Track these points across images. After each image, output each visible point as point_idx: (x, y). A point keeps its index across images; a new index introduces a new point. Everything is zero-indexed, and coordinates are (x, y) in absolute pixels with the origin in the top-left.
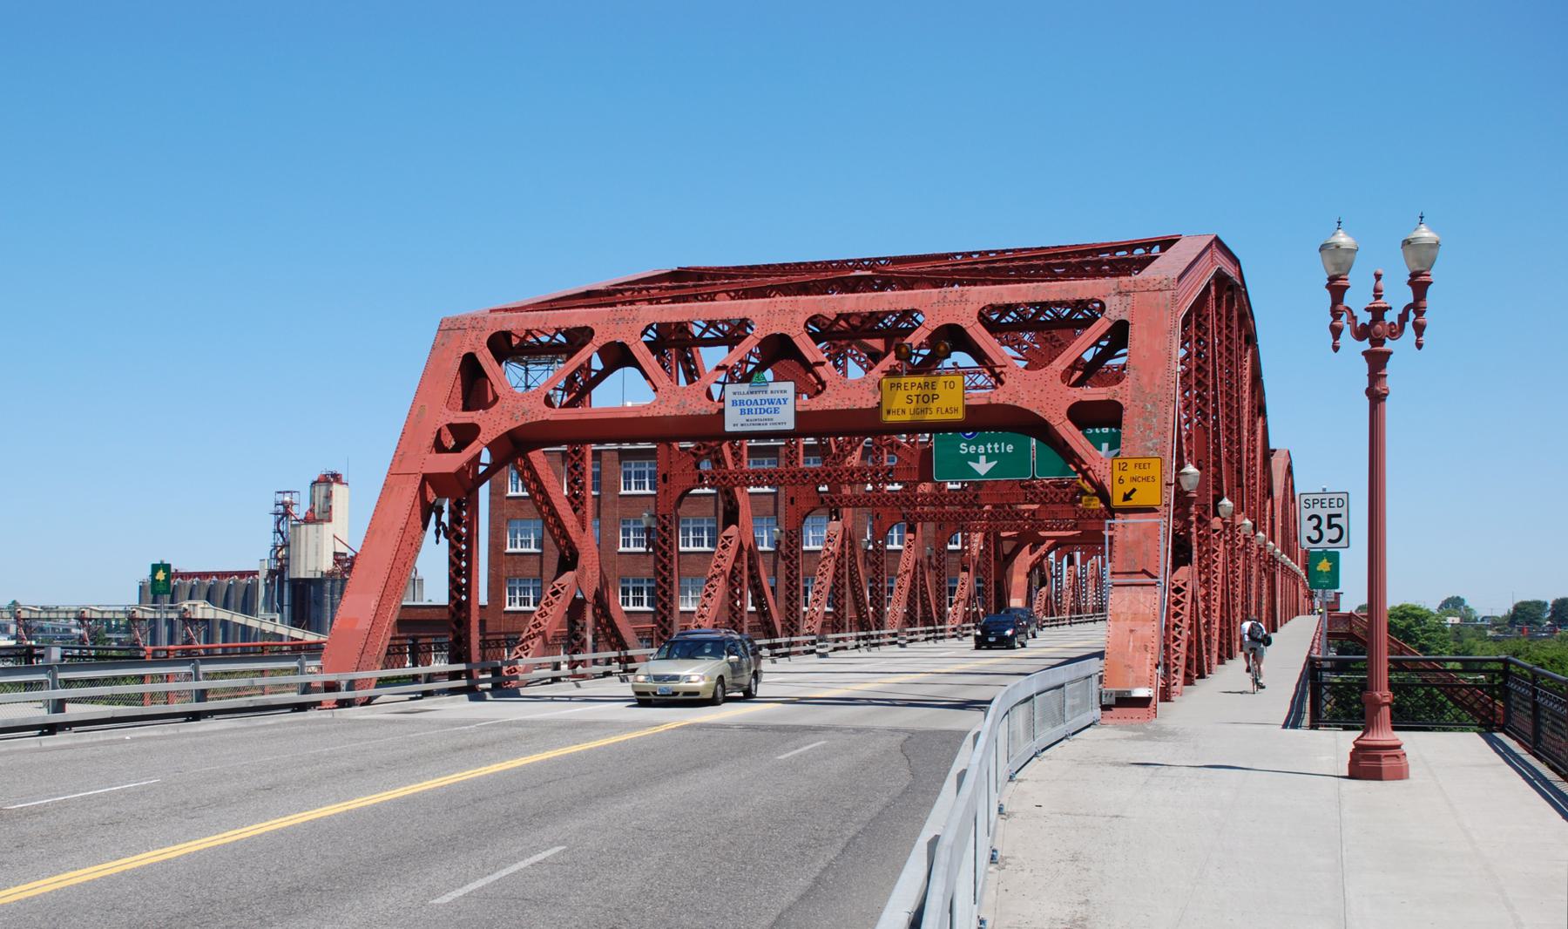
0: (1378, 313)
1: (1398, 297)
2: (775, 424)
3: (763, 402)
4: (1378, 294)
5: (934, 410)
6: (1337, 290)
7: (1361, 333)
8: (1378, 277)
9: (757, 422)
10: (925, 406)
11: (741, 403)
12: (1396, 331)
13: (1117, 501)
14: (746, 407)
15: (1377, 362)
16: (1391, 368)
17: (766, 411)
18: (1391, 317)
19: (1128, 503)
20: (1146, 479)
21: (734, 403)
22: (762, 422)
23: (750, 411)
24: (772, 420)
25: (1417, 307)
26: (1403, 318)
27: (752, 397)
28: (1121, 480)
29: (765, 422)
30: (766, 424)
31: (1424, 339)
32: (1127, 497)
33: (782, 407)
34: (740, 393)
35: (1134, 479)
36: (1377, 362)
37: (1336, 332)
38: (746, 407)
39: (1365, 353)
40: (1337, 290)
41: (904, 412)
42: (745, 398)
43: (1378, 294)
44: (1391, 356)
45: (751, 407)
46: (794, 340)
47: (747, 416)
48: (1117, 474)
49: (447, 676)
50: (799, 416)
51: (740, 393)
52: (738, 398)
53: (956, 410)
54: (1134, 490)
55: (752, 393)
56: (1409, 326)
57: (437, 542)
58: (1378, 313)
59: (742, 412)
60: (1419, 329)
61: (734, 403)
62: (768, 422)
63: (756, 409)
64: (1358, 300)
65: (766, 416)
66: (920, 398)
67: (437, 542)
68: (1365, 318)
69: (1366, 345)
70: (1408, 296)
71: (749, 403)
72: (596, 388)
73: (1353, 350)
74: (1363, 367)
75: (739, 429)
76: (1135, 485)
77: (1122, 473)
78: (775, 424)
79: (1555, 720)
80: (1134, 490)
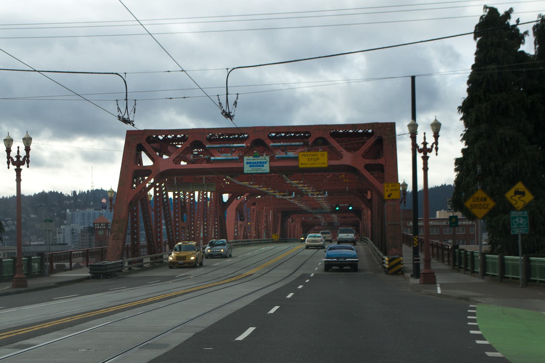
0: (425, 144)
1: (23, 153)
2: (262, 170)
3: (258, 163)
4: (425, 138)
5: (317, 163)
6: (8, 151)
7: (14, 164)
8: (425, 134)
9: (256, 170)
10: (315, 162)
11: (250, 163)
12: (430, 150)
13: (386, 197)
14: (252, 164)
15: (18, 171)
16: (429, 161)
17: (259, 166)
18: (429, 146)
19: (389, 198)
20: (395, 190)
21: (247, 163)
22: (257, 170)
23: (253, 166)
24: (261, 169)
25: (436, 143)
26: (432, 146)
27: (254, 161)
28: (387, 191)
29: (258, 170)
30: (259, 171)
31: (438, 152)
32: (389, 196)
33: (265, 165)
34: (249, 159)
35: (391, 190)
36: (18, 171)
37: (8, 163)
38: (252, 164)
39: (15, 169)
40: (8, 151)
41: (307, 164)
42: (251, 161)
43: (425, 138)
44: (22, 170)
45: (253, 164)
46: (142, 144)
47: (253, 168)
48: (386, 188)
49: (337, 241)
50: (271, 168)
51: (249, 159)
52: (249, 161)
53: (325, 164)
54: (391, 194)
55: (254, 159)
56: (434, 149)
57: (9, 168)
58: (425, 144)
59: (250, 166)
60: (437, 149)
61: (247, 163)
62: (260, 170)
63: (255, 165)
64: (13, 154)
65: (259, 168)
66: (313, 159)
67: (9, 168)
68: (15, 159)
69: (15, 167)
70: (433, 140)
71: (253, 163)
72: (147, 156)
73: (13, 167)
74: (15, 173)
75: (249, 172)
76: (392, 192)
77: (387, 188)
78: (262, 170)
79: (273, 241)
80: (391, 194)
